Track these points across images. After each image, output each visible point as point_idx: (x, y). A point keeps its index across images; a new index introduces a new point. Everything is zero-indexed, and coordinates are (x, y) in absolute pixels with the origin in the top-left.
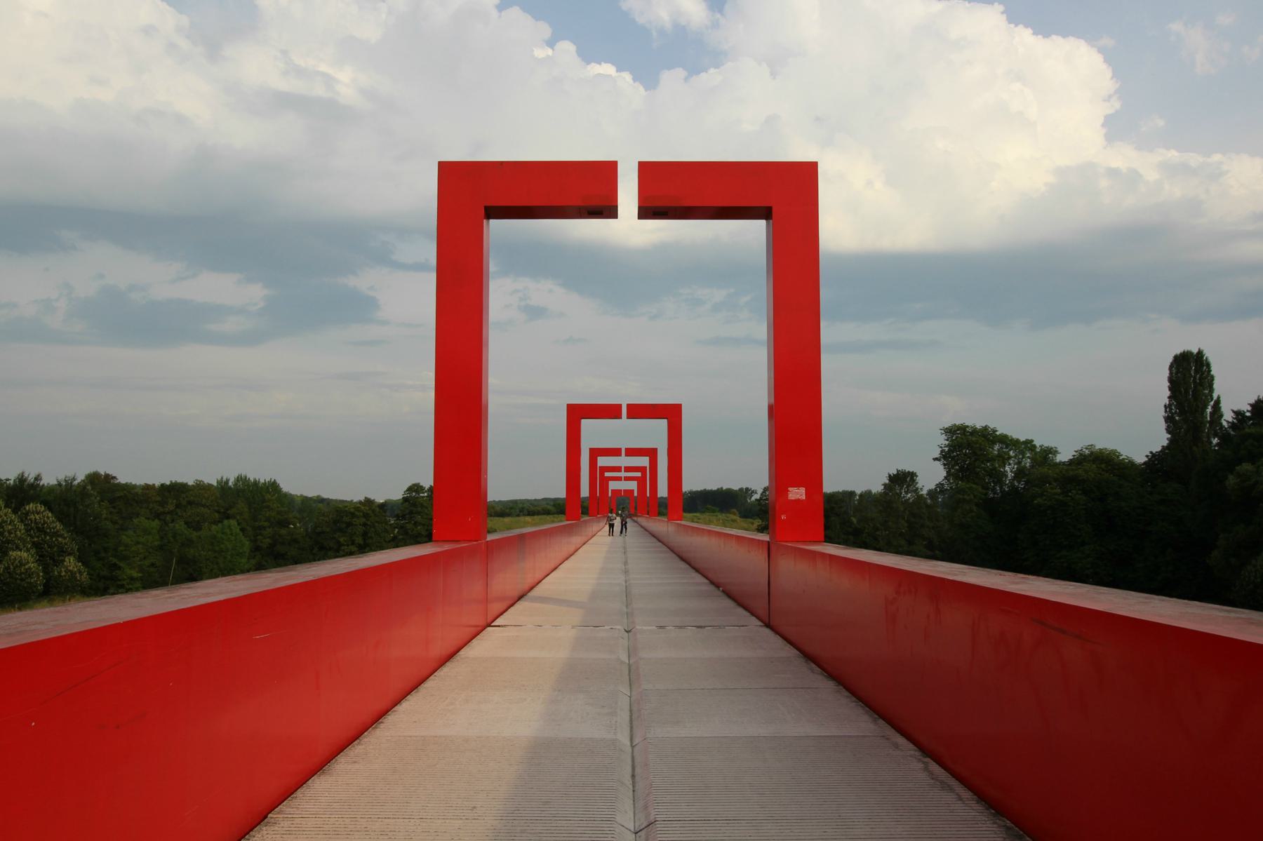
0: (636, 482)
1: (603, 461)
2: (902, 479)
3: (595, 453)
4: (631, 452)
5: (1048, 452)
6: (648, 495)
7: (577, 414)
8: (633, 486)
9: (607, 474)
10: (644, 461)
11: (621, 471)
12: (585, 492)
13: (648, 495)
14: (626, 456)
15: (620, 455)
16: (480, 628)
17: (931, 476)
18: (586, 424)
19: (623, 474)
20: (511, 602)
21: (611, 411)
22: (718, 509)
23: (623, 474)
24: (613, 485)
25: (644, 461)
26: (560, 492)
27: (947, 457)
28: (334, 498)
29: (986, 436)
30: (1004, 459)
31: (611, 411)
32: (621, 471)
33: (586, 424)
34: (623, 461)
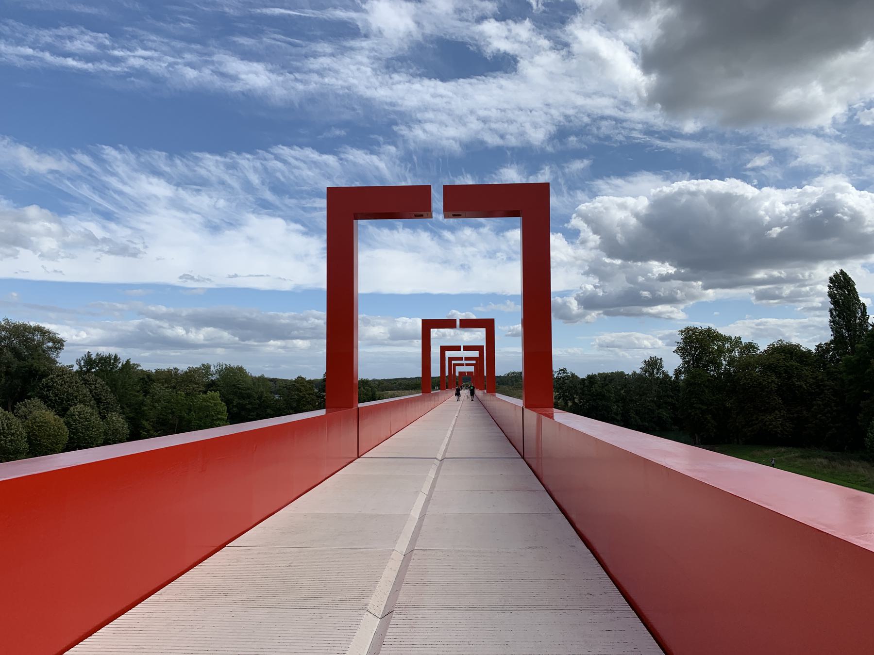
0: (473, 367)
1: (448, 354)
2: (653, 364)
3: (444, 349)
4: (467, 348)
5: (751, 346)
6: (485, 375)
7: (428, 325)
8: (471, 369)
9: (453, 362)
10: (476, 354)
11: (462, 360)
12: (447, 374)
13: (485, 375)
14: (464, 350)
15: (464, 346)
16: (353, 459)
17: (672, 363)
18: (434, 332)
19: (464, 362)
20: (533, 466)
21: (449, 324)
22: (421, 391)
23: (464, 362)
24: (459, 369)
25: (476, 354)
26: (418, 373)
27: (683, 351)
28: (280, 378)
29: (710, 336)
30: (720, 351)
31: (449, 324)
32: (462, 360)
33: (434, 332)
34: (462, 354)
